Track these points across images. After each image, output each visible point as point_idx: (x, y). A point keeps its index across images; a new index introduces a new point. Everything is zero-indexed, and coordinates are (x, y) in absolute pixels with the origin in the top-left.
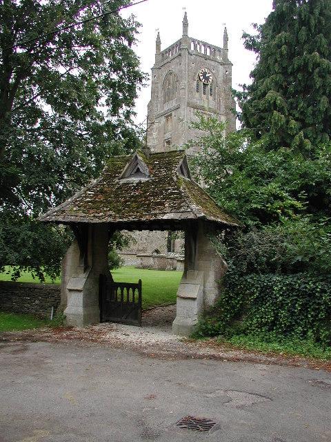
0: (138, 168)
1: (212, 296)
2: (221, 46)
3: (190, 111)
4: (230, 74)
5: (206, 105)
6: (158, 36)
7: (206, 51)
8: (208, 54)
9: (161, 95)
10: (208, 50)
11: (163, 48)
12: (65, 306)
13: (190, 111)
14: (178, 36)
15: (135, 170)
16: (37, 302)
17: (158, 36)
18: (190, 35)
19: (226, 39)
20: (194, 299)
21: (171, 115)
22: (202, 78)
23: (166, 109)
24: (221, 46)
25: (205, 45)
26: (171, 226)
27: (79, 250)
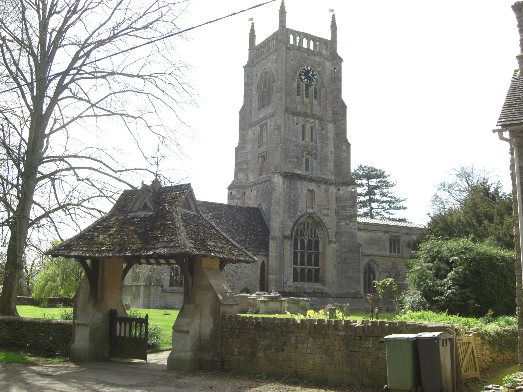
0: (145, 203)
1: (207, 331)
2: (328, 37)
3: (289, 119)
4: (340, 71)
5: (309, 111)
6: (253, 26)
7: (308, 44)
8: (312, 48)
9: (255, 98)
10: (312, 43)
11: (258, 41)
12: (74, 342)
13: (289, 119)
14: (275, 28)
15: (143, 204)
16: (51, 338)
17: (253, 26)
18: (290, 25)
19: (334, 27)
20: (87, 325)
21: (266, 124)
22: (303, 77)
23: (261, 116)
24: (328, 37)
25: (309, 37)
26: (167, 258)
27: (89, 285)
